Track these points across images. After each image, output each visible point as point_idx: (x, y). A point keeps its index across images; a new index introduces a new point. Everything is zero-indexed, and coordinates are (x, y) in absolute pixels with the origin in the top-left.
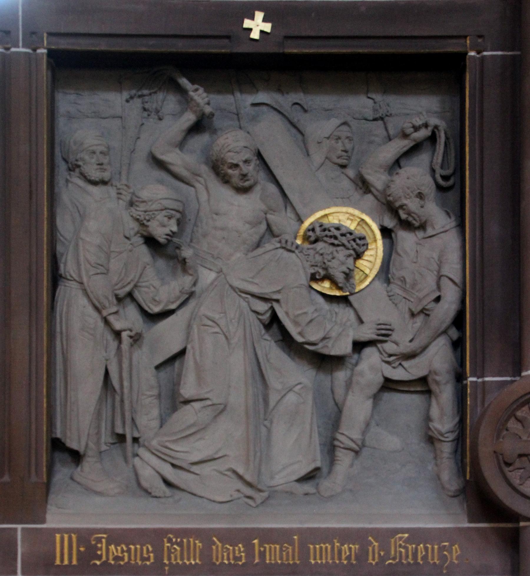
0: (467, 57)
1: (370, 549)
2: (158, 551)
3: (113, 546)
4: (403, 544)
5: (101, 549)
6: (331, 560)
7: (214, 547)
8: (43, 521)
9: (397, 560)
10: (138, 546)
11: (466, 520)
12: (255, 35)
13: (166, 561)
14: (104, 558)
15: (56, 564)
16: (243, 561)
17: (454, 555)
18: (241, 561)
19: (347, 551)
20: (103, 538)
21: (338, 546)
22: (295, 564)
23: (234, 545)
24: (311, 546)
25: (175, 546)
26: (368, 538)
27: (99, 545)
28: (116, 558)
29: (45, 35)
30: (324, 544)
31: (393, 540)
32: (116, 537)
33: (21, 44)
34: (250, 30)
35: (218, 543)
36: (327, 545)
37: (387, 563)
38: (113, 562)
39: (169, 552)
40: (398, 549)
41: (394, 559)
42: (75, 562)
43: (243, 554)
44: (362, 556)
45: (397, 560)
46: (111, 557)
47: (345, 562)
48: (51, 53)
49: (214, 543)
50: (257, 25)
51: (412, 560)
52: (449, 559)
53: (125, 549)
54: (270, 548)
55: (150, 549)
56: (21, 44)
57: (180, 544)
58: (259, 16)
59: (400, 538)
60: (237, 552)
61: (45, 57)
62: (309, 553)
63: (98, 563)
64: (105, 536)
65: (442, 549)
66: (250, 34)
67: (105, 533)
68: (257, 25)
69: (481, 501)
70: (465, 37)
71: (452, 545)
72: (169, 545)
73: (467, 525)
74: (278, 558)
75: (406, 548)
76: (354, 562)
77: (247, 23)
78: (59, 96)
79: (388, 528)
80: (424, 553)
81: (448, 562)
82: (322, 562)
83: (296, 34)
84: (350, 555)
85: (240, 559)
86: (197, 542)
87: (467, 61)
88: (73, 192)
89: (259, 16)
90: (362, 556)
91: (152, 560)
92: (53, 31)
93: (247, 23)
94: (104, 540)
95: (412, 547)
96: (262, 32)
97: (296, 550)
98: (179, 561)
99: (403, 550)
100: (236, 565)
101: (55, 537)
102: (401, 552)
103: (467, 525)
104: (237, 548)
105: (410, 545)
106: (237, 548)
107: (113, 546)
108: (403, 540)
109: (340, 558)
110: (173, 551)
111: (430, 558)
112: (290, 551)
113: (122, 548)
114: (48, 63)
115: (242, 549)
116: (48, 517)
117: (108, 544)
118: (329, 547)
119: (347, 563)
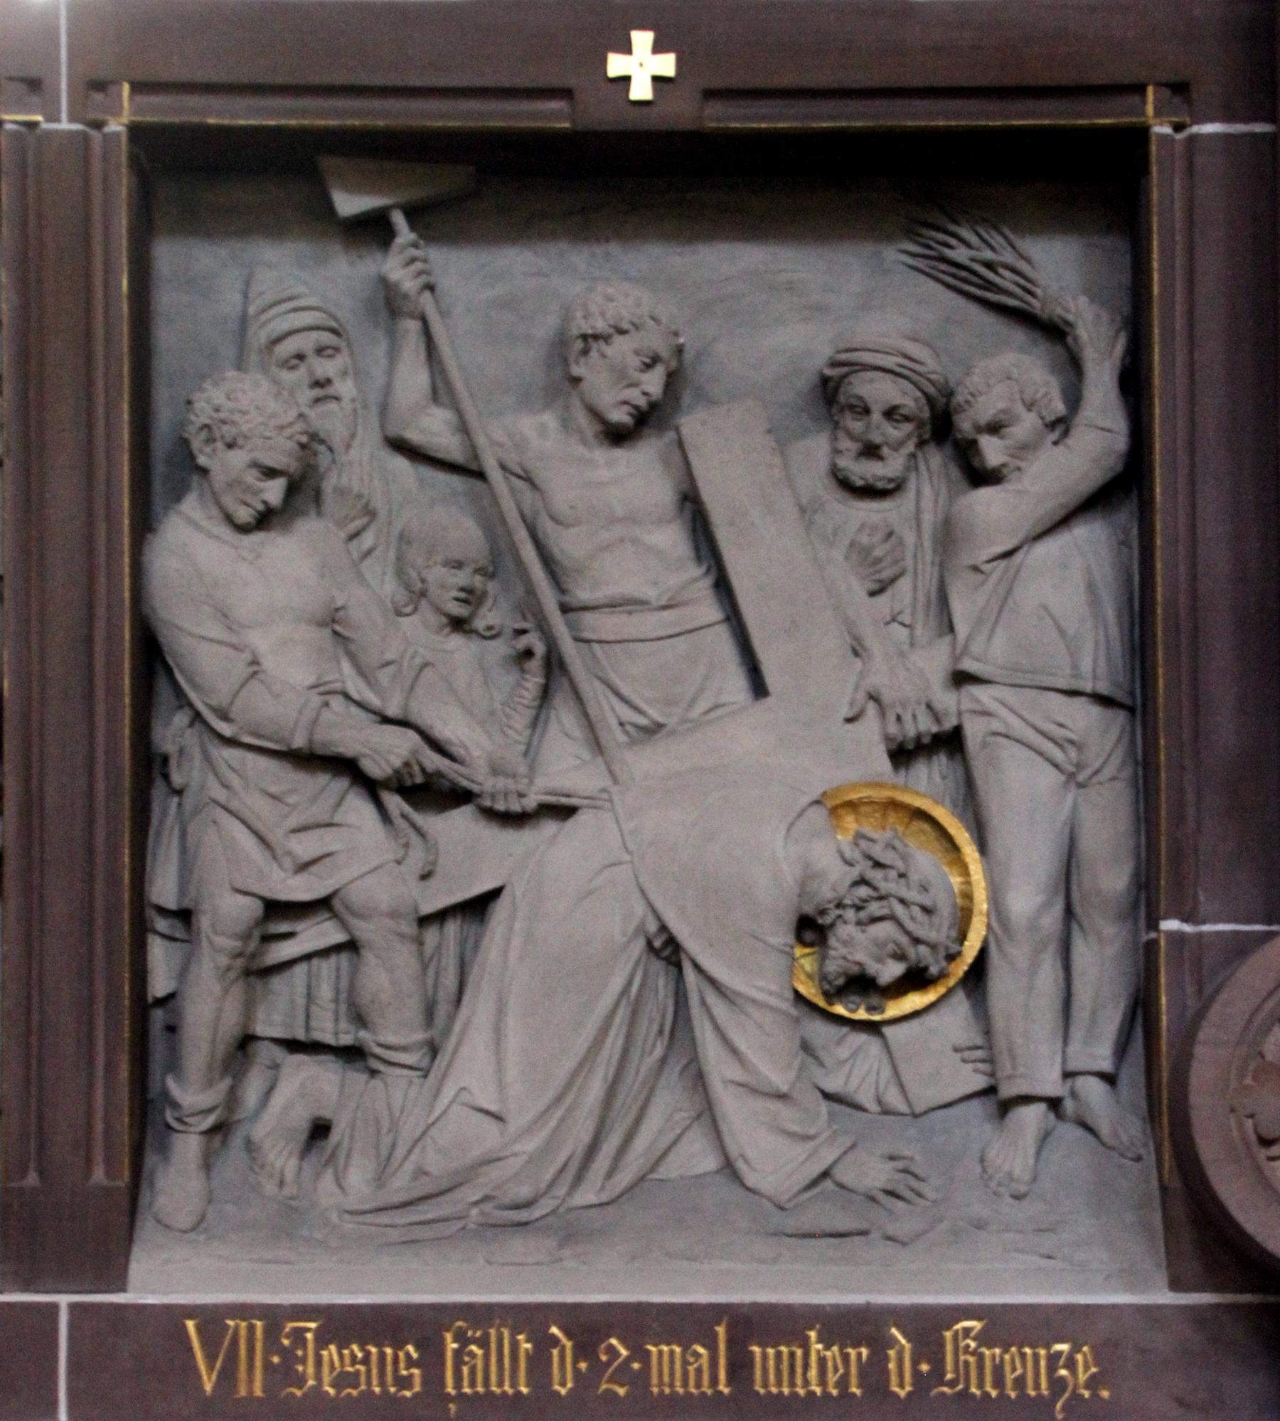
0: (1153, 138)
1: (555, 1352)
2: (740, 1367)
3: (333, 1348)
4: (973, 1344)
5: (303, 1361)
6: (1014, 1389)
7: (892, 1353)
8: (122, 1289)
9: (363, 1387)
10: (389, 1351)
11: (1162, 1278)
12: (641, 90)
13: (450, 1390)
14: (311, 1382)
15: (237, 1396)
16: (417, 1389)
17: (1082, 1377)
18: (356, 1387)
19: (839, 1361)
20: (309, 1330)
21: (818, 1352)
22: (518, 1394)
23: (398, 1345)
24: (756, 1349)
25: (473, 1348)
26: (549, 1327)
27: (300, 1353)
28: (343, 1380)
29: (126, 88)
30: (668, 1344)
31: (948, 1335)
32: (343, 1324)
33: (64, 116)
34: (626, 80)
35: (564, 1340)
36: (794, 1349)
37: (726, 1391)
38: (332, 1391)
39: (458, 1363)
40: (962, 1358)
41: (952, 1384)
42: (258, 1392)
43: (416, 1371)
44: (874, 1373)
45: (960, 1387)
46: (326, 1378)
47: (1013, 1395)
48: (137, 132)
49: (893, 1342)
50: (642, 65)
51: (454, 1388)
52: (1070, 1388)
53: (360, 1355)
54: (779, 1355)
55: (415, 1355)
56: (64, 116)
57: (484, 1343)
58: (642, 39)
59: (967, 1331)
60: (402, 1365)
61: (124, 139)
62: (530, 1371)
63: (354, 1393)
64: (313, 1325)
65: (1053, 1359)
66: (628, 90)
67: (979, 1319)
68: (642, 65)
69: (1202, 1233)
70: (1140, 89)
71: (1076, 1349)
72: (820, 1346)
73: (1167, 1297)
74: (678, 1383)
75: (981, 1358)
76: (726, 1391)
77: (616, 65)
78: (168, 255)
79: (922, 1305)
80: (841, 1371)
81: (1066, 1395)
82: (662, 1392)
83: (477, 82)
84: (846, 1376)
85: (405, 1383)
86: (521, 1337)
87: (1154, 148)
88: (195, 557)
89: (642, 39)
90: (874, 1373)
91: (417, 1389)
92: (718, 83)
93: (616, 65)
94: (309, 1336)
95: (993, 1357)
96: (657, 80)
97: (722, 1362)
98: (507, 1388)
99: (971, 1359)
100: (395, 1400)
101: (185, 1327)
102: (966, 1363)
103: (1167, 1297)
104: (346, 1352)
105: (989, 1348)
106: (401, 1355)
107: (333, 1348)
108: (973, 1334)
109: (999, 1382)
110: (466, 1359)
111: (1030, 1381)
112: (705, 1362)
113: (408, 1355)
114: (134, 162)
115: (415, 1355)
116: (141, 1265)
117: (322, 1342)
118: (799, 1352)
119: (1018, 1397)
